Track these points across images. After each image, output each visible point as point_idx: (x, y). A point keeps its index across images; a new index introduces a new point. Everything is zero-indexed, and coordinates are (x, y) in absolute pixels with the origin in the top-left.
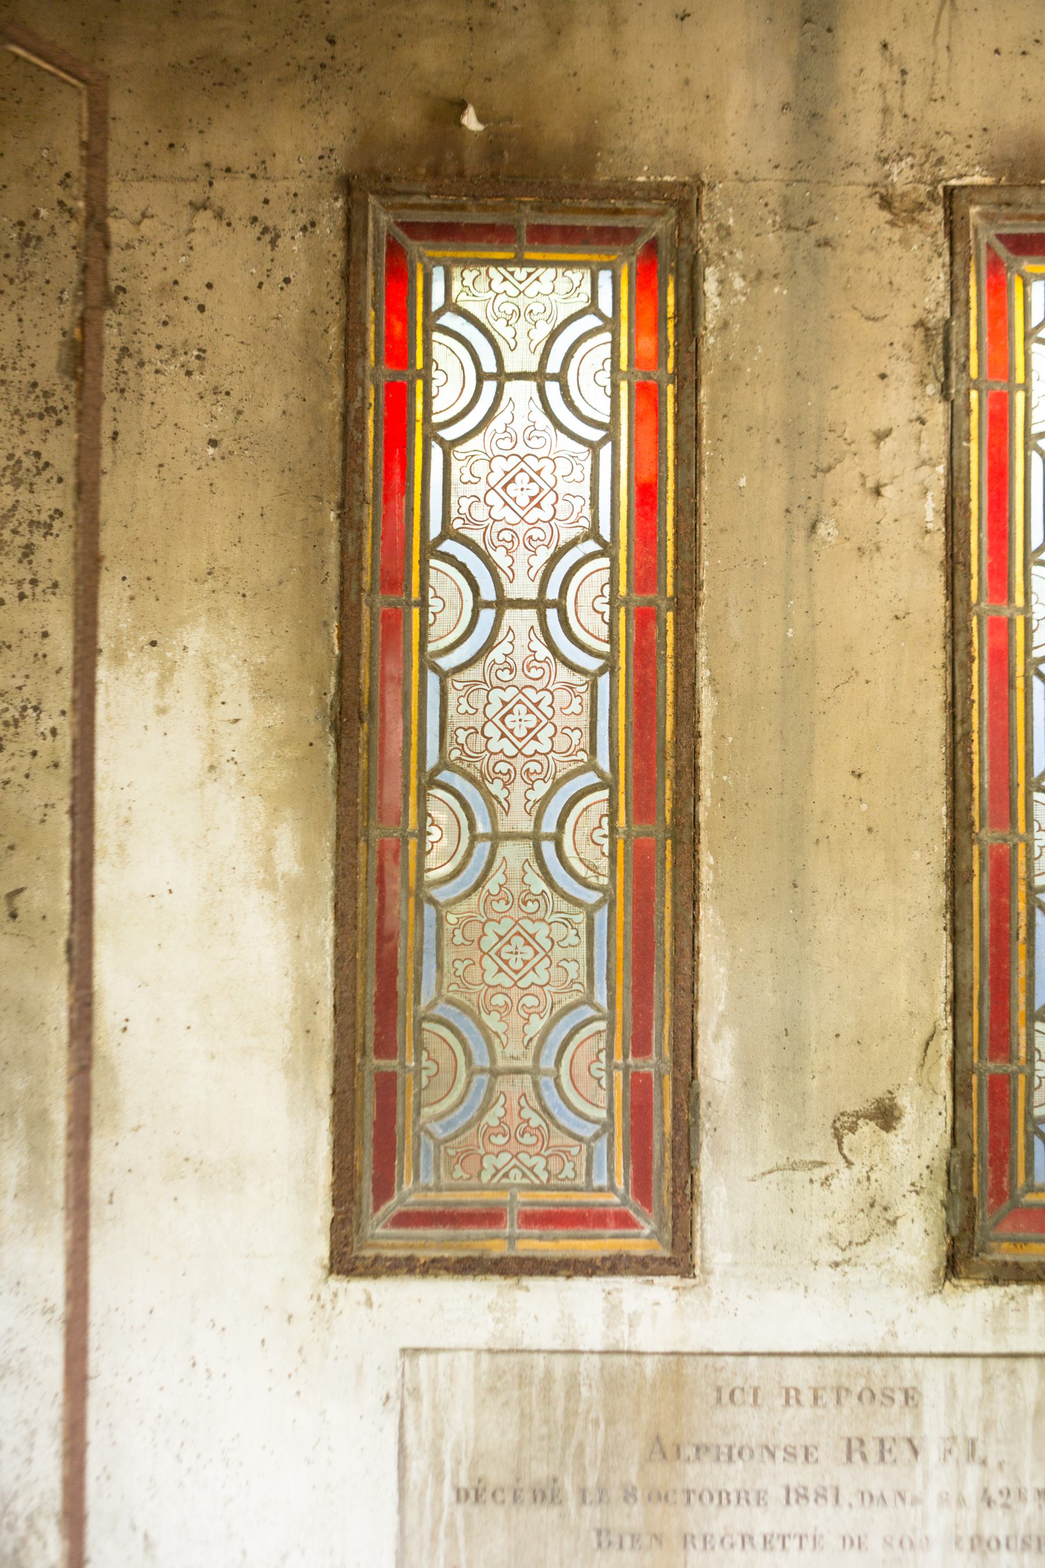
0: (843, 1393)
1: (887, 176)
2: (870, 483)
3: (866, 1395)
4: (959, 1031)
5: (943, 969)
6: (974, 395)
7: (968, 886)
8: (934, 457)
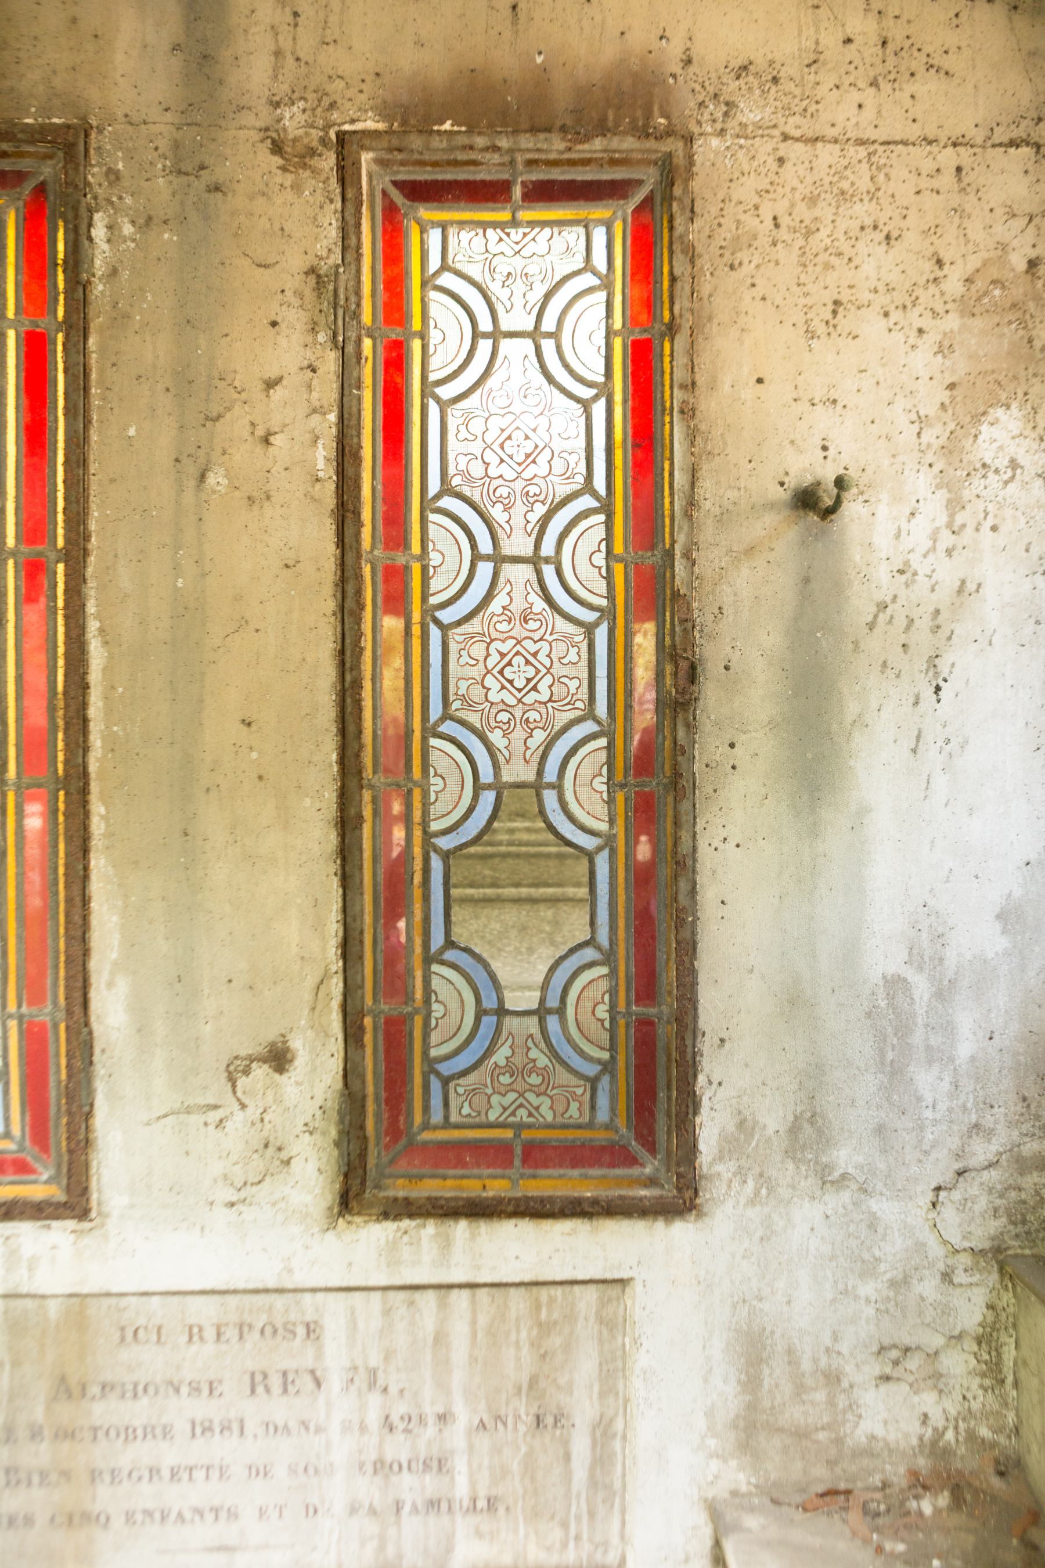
0: (246, 1329)
1: (279, 121)
2: (260, 432)
3: (268, 1330)
4: (348, 974)
5: (334, 914)
6: (367, 343)
7: (357, 832)
8: (326, 405)
